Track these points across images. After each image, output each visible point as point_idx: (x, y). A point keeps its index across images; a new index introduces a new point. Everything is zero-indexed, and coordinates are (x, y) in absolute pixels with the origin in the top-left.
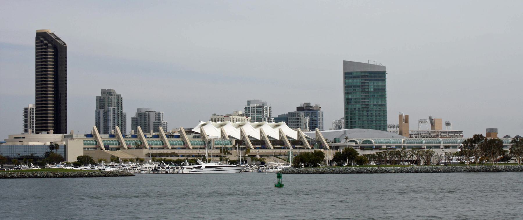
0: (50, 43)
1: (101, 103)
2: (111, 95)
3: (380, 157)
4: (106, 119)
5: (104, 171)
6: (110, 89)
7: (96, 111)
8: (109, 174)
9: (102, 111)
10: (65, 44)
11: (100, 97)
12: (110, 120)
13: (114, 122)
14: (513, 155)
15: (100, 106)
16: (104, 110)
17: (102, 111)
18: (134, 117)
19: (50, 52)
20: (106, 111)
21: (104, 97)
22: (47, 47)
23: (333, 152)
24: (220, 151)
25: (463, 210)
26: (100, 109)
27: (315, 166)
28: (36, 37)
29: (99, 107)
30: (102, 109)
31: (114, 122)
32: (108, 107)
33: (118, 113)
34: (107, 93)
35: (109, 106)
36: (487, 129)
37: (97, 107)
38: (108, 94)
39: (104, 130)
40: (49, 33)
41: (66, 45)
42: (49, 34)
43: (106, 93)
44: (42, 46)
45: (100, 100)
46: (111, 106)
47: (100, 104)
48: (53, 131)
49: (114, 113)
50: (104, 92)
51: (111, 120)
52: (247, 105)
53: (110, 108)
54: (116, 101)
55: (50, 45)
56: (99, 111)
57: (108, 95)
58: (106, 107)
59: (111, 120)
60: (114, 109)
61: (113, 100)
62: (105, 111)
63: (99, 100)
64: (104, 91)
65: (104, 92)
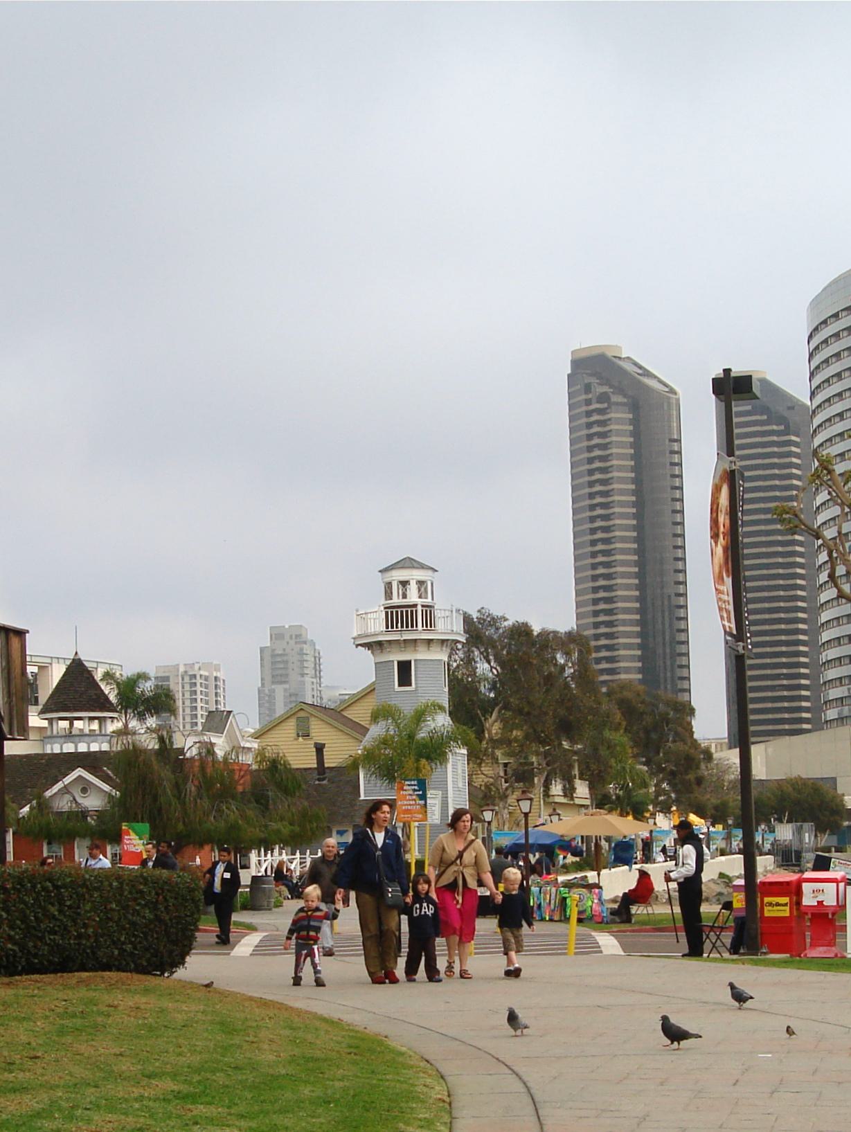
0: (621, 391)
5: (503, 684)
9: (280, 691)
10: (673, 391)
16: (287, 686)
18: (532, 631)
19: (619, 421)
20: (292, 691)
21: (284, 650)
22: (605, 405)
24: (590, 789)
26: (273, 683)
28: (569, 376)
29: (268, 679)
32: (300, 679)
40: (615, 357)
41: (675, 393)
42: (616, 361)
43: (287, 638)
44: (588, 402)
45: (273, 656)
47: (273, 676)
52: (757, 778)
55: (616, 399)
57: (292, 642)
63: (268, 659)
65: (277, 634)
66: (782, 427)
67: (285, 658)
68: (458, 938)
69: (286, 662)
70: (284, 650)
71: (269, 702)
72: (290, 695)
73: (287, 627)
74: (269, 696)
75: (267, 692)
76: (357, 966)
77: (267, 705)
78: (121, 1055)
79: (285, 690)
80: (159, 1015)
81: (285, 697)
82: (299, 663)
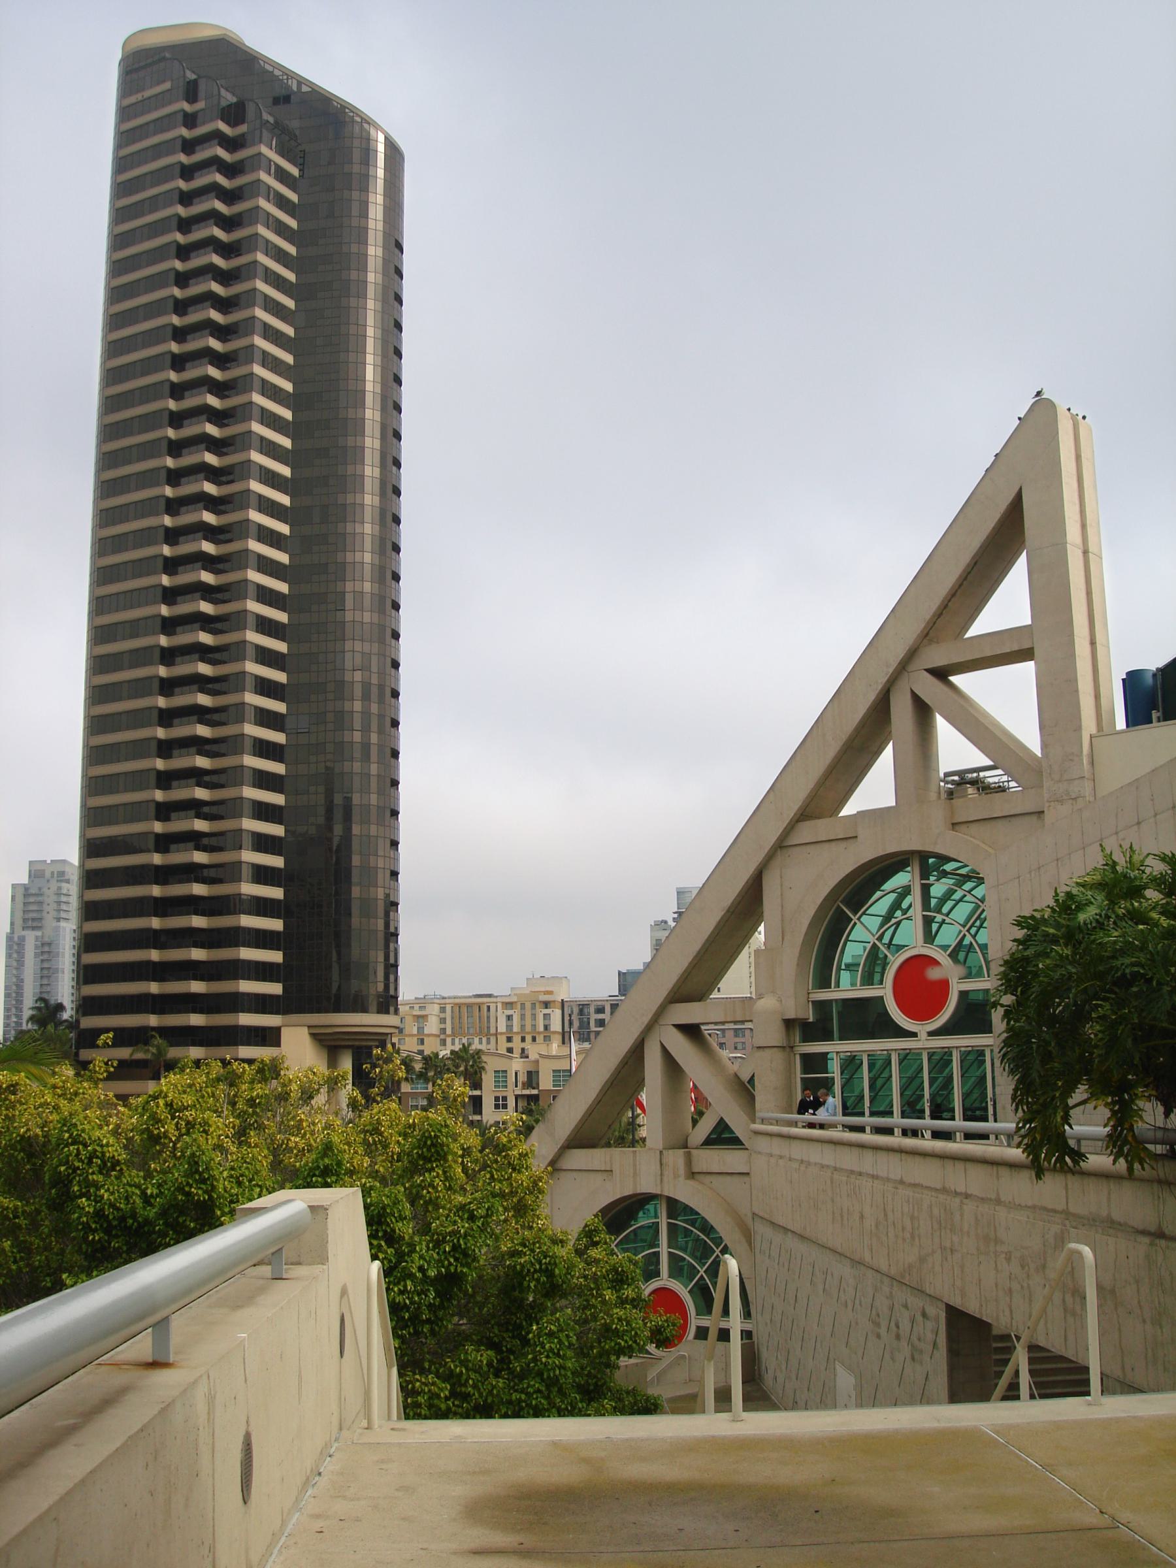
1: (464, 1010)
3: (419, 1196)
4: (46, 965)
7: (10, 938)
9: (31, 937)
11: (26, 888)
14: (207, 1197)
15: (25, 920)
16: (39, 933)
17: (31, 937)
20: (46, 939)
21: (40, 889)
25: (1004, 1108)
27: (1026, 1144)
29: (19, 922)
30: (34, 928)
32: (55, 924)
35: (58, 919)
36: (31, 862)
37: (12, 924)
39: (38, 991)
45: (26, 895)
53: (64, 928)
56: (22, 939)
58: (49, 921)
62: (42, 937)
63: (20, 899)
64: (39, 867)
66: (295, 172)
67: (40, 899)
68: (624, 1361)
69: (41, 903)
70: (40, 889)
71: (18, 952)
72: (43, 945)
73: (49, 862)
74: (18, 944)
75: (16, 939)
76: (229, 564)
77: (15, 955)
78: (833, 1201)
79: (37, 938)
80: (551, 1355)
81: (36, 947)
82: (55, 905)
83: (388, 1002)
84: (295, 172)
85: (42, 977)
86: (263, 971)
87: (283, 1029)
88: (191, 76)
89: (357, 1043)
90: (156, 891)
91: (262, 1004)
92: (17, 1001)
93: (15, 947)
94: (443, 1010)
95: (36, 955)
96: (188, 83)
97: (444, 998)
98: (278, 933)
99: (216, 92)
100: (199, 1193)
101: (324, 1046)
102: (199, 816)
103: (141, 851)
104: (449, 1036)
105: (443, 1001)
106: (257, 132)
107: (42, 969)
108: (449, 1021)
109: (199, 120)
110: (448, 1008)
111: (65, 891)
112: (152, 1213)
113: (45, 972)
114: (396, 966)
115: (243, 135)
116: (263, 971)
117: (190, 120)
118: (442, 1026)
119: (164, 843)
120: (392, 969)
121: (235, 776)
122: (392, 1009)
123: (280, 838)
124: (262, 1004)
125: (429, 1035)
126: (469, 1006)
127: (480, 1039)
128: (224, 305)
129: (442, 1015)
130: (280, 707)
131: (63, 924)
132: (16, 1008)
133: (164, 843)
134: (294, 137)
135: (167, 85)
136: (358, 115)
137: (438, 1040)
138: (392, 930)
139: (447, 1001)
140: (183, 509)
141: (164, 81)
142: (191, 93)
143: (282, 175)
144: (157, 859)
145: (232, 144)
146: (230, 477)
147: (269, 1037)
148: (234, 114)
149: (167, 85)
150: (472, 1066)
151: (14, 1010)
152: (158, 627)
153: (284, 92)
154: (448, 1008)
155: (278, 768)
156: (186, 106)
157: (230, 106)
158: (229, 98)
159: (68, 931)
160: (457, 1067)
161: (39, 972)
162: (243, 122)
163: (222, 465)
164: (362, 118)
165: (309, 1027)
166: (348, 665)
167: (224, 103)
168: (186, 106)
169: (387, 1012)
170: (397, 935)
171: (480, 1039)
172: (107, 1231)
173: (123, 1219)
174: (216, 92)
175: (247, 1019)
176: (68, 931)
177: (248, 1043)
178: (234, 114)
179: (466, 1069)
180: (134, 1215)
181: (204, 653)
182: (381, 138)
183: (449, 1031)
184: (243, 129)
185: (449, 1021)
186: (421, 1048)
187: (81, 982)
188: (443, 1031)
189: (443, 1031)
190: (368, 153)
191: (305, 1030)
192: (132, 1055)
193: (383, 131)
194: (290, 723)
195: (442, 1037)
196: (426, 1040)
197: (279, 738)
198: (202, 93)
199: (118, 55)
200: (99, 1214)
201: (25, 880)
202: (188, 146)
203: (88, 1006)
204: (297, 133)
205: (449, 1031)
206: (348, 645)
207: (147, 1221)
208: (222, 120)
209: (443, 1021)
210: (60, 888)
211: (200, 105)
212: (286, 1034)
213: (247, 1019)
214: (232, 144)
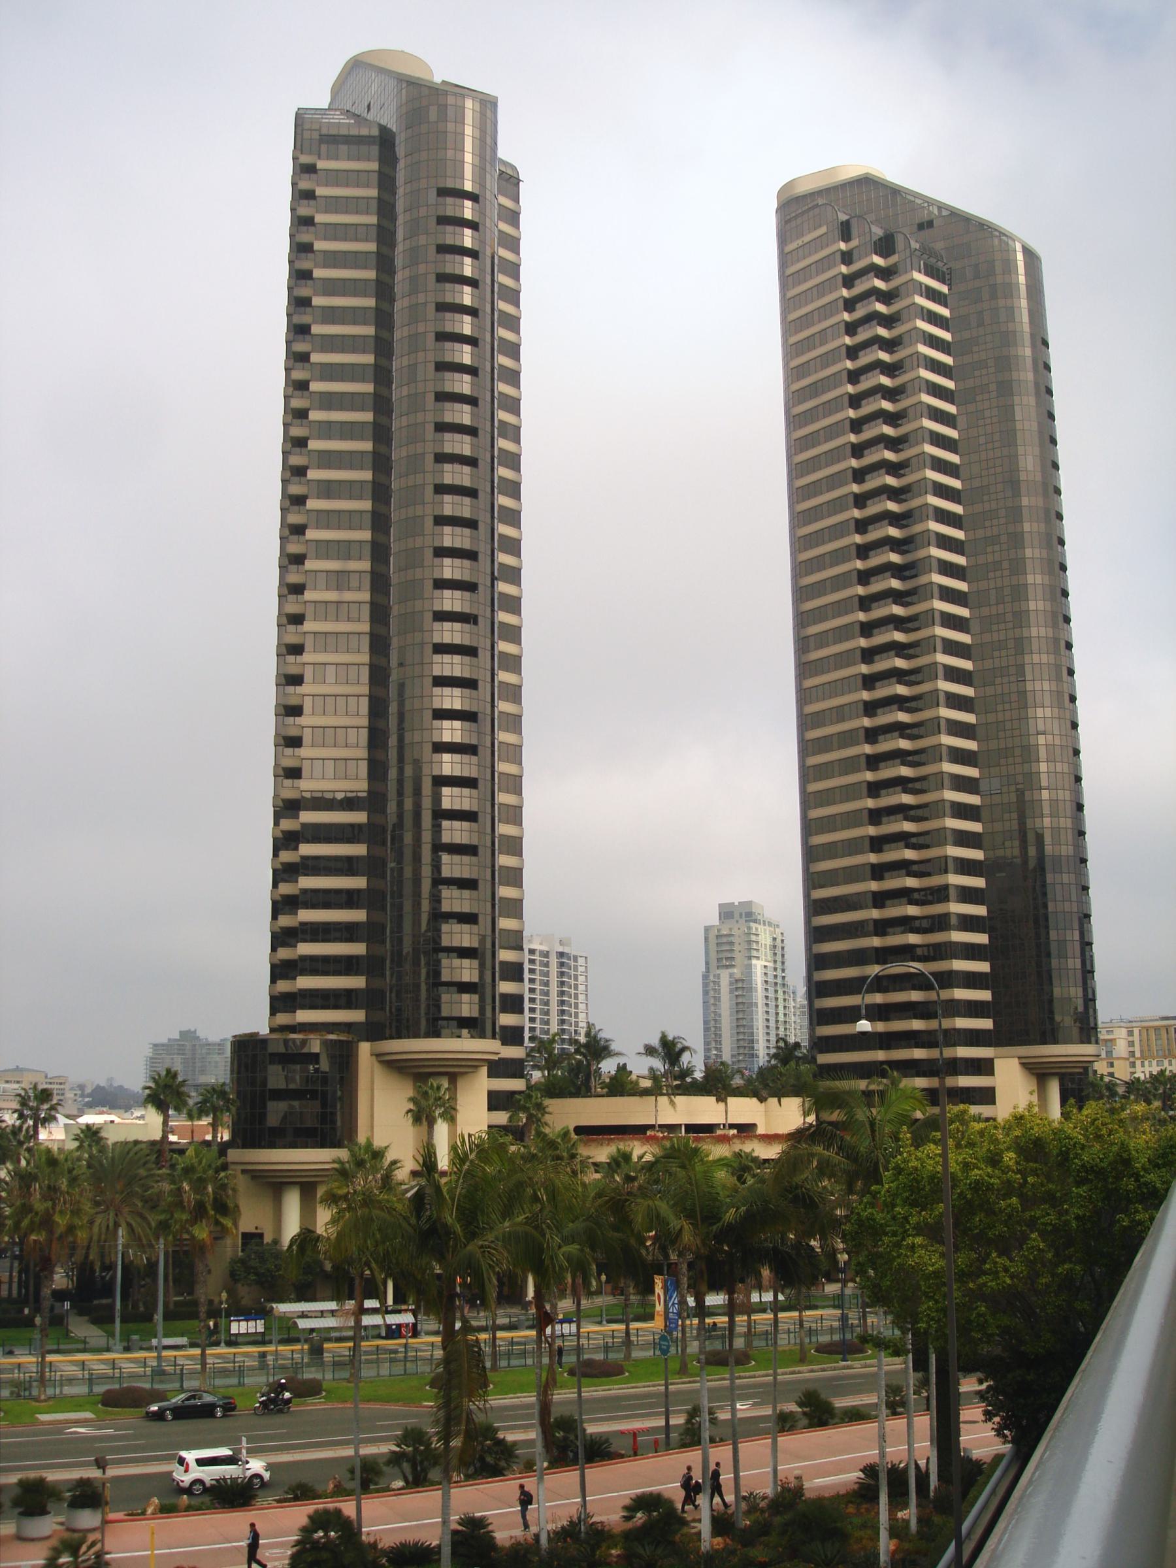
2: (755, 921)
4: (740, 1000)
6: (750, 903)
7: (705, 977)
8: (1101, 1160)
9: (725, 977)
12: (756, 991)
13: (768, 1020)
15: (719, 960)
23: (424, 1351)
31: (768, 1027)
32: (746, 962)
33: (775, 947)
34: (741, 915)
37: (707, 963)
38: (744, 919)
39: (735, 1024)
43: (736, 915)
46: (758, 958)
48: (153, 1143)
49: (768, 1027)
50: (727, 913)
51: (760, 1005)
53: (755, 965)
54: (769, 942)
59: (760, 1021)
60: (765, 967)
61: (762, 939)
66: (945, 289)
73: (737, 904)
79: (731, 975)
81: (731, 983)
83: (1087, 1030)
84: (945, 289)
85: (737, 1012)
86: (974, 1009)
87: (995, 1061)
88: (843, 217)
89: (1063, 1071)
90: (876, 942)
91: (974, 1038)
92: (716, 1035)
93: (709, 986)
94: (1131, 1033)
95: (731, 991)
96: (842, 223)
97: (1130, 1022)
98: (986, 974)
99: (867, 230)
100: (1125, 1155)
101: (1033, 1074)
102: (909, 874)
103: (861, 908)
104: (1138, 1059)
105: (1129, 1025)
106: (908, 260)
107: (737, 1004)
108: (1137, 1044)
109: (855, 257)
110: (1136, 1031)
111: (754, 931)
112: (1104, 1165)
113: (741, 1006)
114: (1094, 1000)
115: (895, 265)
116: (974, 1009)
117: (847, 258)
118: (1131, 1049)
119: (880, 899)
120: (1091, 1003)
121: (938, 837)
122: (1093, 1039)
123: (981, 890)
124: (974, 1038)
125: (1118, 1058)
126: (1157, 1029)
127: (1170, 1061)
128: (893, 419)
129: (1130, 1039)
130: (972, 772)
131: (754, 961)
132: (716, 1041)
133: (880, 899)
134: (939, 258)
135: (823, 230)
136: (996, 230)
137: (1128, 1062)
138: (1089, 968)
139: (1134, 1024)
140: (874, 605)
141: (820, 226)
142: (845, 232)
143: (932, 295)
144: (875, 914)
145: (885, 274)
146: (913, 572)
147: (984, 1067)
148: (885, 246)
149: (823, 230)
150: (1170, 1089)
151: (713, 1044)
152: (861, 711)
153: (926, 218)
154: (1136, 1031)
155: (975, 827)
156: (843, 246)
157: (880, 239)
158: (878, 232)
159: (759, 967)
160: (1156, 1089)
161: (735, 1007)
162: (894, 253)
163: (906, 562)
164: (1000, 232)
165: (1019, 1058)
166: (1032, 731)
167: (875, 238)
168: (843, 246)
169: (1089, 1042)
170: (1093, 972)
171: (1170, 1061)
172: (1086, 1172)
173: (1092, 1167)
174: (867, 230)
175: (963, 1052)
176: (759, 967)
177: (967, 1073)
178: (885, 246)
179: (1164, 1092)
180: (1096, 1165)
181: (901, 729)
182: (1018, 247)
183: (1138, 1055)
184: (893, 259)
185: (1137, 1044)
186: (1111, 1070)
187: (815, 1022)
188: (1132, 1054)
189: (1132, 1054)
190: (1009, 266)
191: (1016, 1060)
192: (867, 1086)
193: (1020, 241)
194: (983, 786)
195: (1132, 1059)
196: (1116, 1063)
197: (974, 800)
198: (854, 231)
199: (774, 205)
200: (1083, 1166)
201: (714, 920)
202: (848, 281)
203: (984, 1067)
204: (943, 253)
205: (1138, 1055)
206: (1031, 712)
207: (1103, 1168)
208: (876, 254)
209: (1131, 1044)
210: (749, 928)
211: (854, 243)
212: (998, 1063)
213: (963, 1052)
214: (885, 274)
